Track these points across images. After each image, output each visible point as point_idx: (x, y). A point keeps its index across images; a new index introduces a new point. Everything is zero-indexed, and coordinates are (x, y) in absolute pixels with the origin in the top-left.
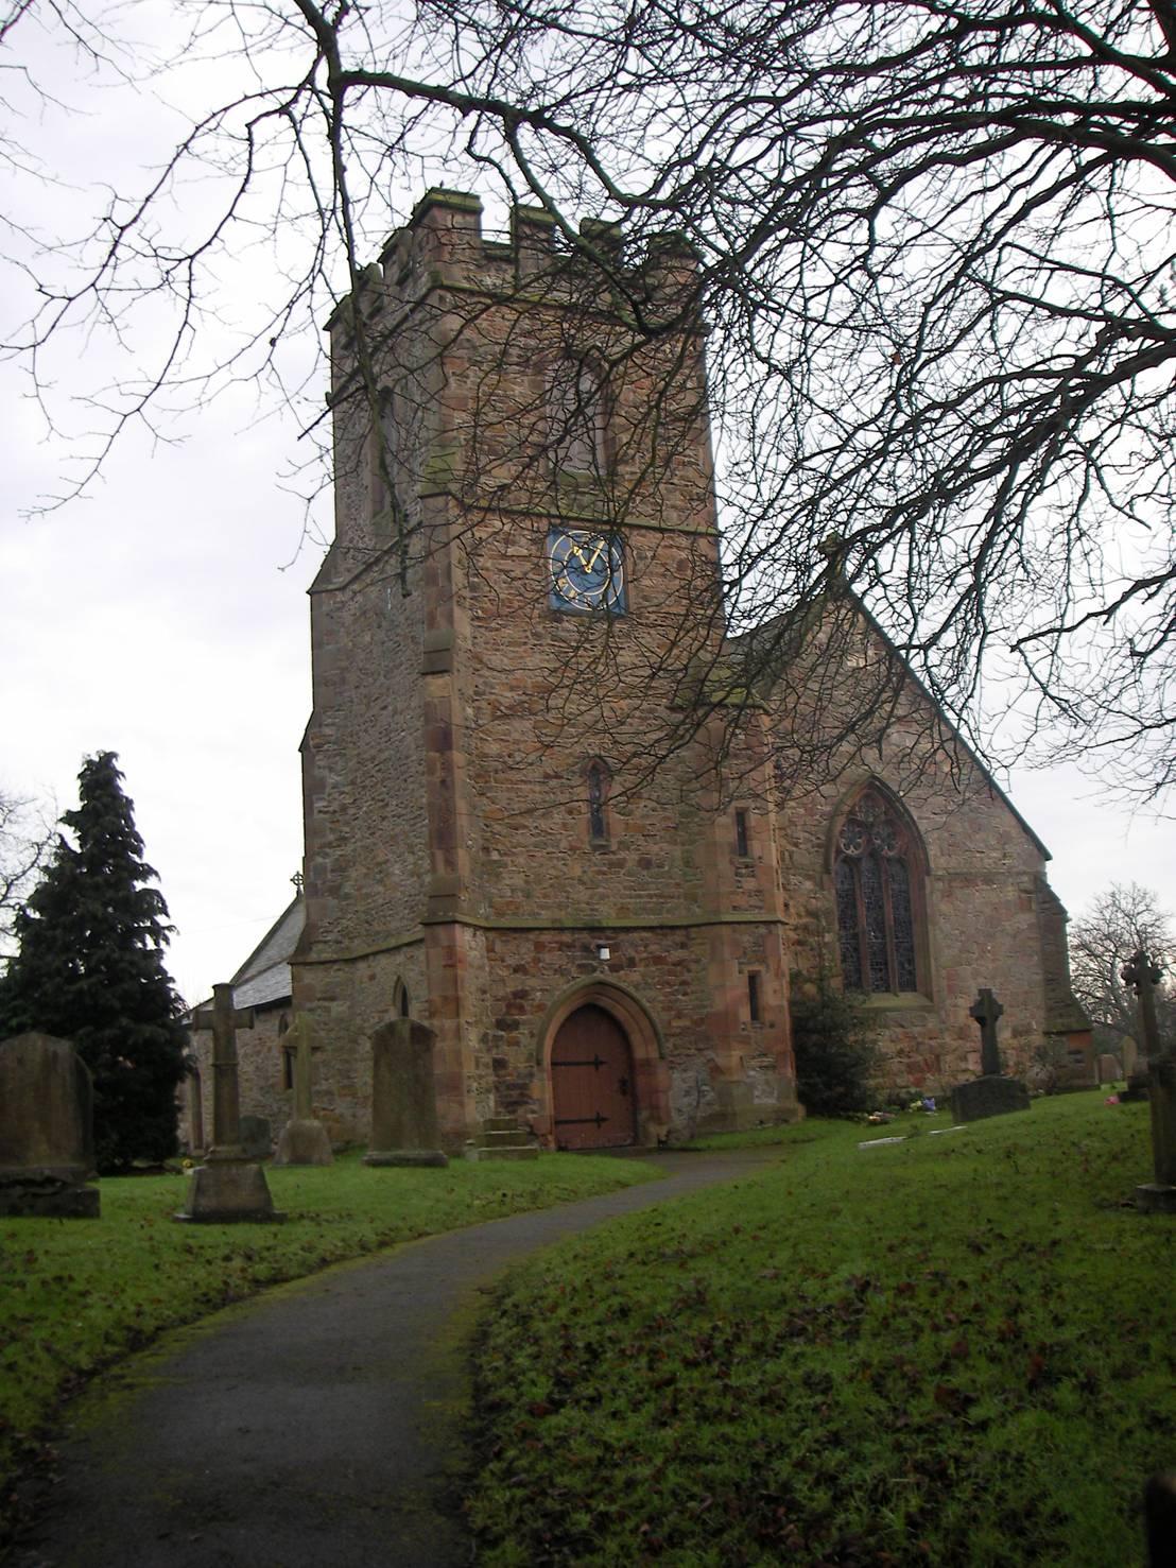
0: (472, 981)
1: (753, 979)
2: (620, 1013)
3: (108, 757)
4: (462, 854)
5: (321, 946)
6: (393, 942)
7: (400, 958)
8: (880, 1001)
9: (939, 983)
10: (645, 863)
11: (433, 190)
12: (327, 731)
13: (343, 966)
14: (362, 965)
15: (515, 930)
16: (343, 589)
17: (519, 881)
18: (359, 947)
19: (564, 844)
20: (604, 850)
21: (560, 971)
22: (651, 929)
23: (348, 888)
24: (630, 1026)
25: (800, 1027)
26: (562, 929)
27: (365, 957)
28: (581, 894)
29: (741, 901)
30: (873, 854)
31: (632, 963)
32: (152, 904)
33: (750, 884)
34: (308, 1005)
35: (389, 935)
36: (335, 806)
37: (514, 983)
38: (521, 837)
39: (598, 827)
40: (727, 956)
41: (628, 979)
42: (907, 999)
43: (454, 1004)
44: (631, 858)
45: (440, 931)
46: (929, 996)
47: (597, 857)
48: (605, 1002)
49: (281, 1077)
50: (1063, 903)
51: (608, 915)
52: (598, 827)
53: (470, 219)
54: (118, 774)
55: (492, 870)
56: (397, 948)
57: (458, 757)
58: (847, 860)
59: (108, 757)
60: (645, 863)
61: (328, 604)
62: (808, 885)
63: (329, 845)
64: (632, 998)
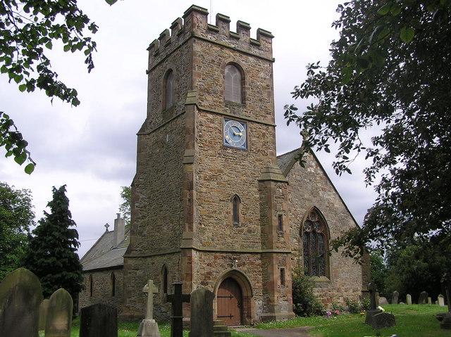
0: (196, 267)
1: (282, 270)
2: (239, 281)
3: (63, 188)
4: (194, 225)
5: (134, 252)
6: (162, 252)
7: (165, 258)
8: (317, 279)
9: (332, 275)
10: (249, 231)
11: (193, 5)
12: (141, 180)
13: (143, 259)
14: (149, 259)
15: (208, 251)
16: (149, 134)
17: (210, 234)
18: (148, 253)
19: (225, 224)
20: (237, 226)
21: (222, 266)
22: (251, 253)
23: (145, 233)
24: (242, 285)
25: (294, 288)
26: (223, 252)
27: (150, 256)
28: (229, 240)
29: (279, 245)
30: (314, 232)
31: (244, 264)
32: (74, 234)
33: (282, 240)
34: (129, 271)
35: (160, 249)
36: (142, 205)
37: (207, 269)
38: (212, 220)
39: (236, 218)
40: (274, 263)
41: (243, 269)
42: (323, 278)
43: (190, 276)
44: (245, 229)
45: (187, 251)
46: (329, 278)
47: (235, 228)
48: (234, 277)
49: (110, 293)
50: (70, 203)
51: (237, 248)
52: (236, 218)
53: (267, 65)
54: (66, 190)
55: (202, 231)
56: (164, 255)
57: (194, 192)
58: (306, 233)
59: (63, 188)
60: (249, 231)
61: (144, 139)
62: (295, 240)
63: (139, 218)
64: (244, 276)
